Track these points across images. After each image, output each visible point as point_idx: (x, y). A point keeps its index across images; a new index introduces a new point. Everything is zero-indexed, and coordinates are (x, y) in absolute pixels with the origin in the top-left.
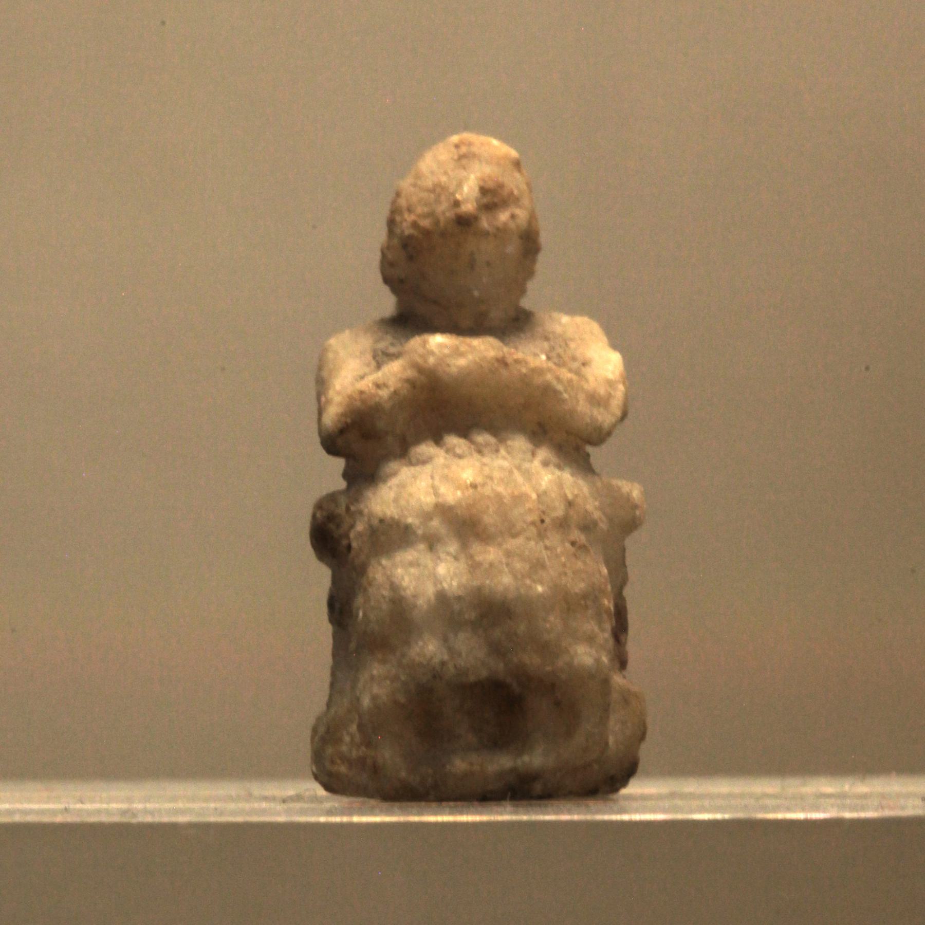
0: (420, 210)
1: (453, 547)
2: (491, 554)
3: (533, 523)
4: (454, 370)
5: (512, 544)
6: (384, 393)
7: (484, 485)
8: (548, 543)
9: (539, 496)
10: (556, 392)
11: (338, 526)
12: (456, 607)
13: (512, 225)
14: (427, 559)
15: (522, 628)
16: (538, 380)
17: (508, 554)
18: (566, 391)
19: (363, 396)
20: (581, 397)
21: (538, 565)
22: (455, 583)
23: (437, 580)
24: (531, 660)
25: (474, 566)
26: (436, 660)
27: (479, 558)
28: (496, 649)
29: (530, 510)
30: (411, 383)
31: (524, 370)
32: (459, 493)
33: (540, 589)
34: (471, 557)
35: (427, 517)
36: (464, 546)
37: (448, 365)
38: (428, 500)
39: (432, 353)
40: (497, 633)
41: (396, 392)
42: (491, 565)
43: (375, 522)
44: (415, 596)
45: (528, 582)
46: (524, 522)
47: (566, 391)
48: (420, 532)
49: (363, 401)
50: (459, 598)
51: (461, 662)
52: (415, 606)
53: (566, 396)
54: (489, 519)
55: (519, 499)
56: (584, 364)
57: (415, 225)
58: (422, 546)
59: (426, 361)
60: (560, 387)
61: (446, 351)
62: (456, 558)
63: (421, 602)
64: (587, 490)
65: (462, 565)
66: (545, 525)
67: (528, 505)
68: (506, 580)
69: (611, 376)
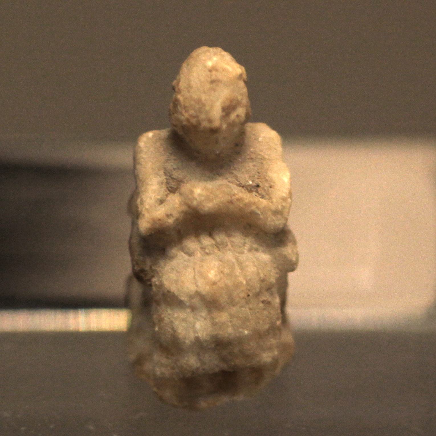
0: (192, 112)
1: (204, 313)
2: (223, 317)
3: (244, 298)
4: (206, 209)
5: (234, 310)
6: (171, 221)
7: (219, 281)
8: (251, 306)
9: (247, 282)
10: (257, 214)
11: (146, 275)
12: (205, 344)
13: (237, 121)
14: (191, 317)
15: (236, 350)
16: (249, 210)
17: (231, 316)
18: (262, 214)
19: (161, 222)
20: (270, 213)
21: (246, 320)
22: (204, 334)
23: (195, 332)
24: (239, 362)
25: (214, 324)
26: (195, 367)
27: (217, 320)
28: (223, 359)
29: (243, 291)
30: (185, 213)
31: (241, 205)
32: (208, 287)
33: (246, 332)
34: (212, 319)
35: (191, 297)
36: (210, 312)
37: (204, 206)
38: (192, 288)
39: (195, 199)
40: (224, 353)
41: (177, 219)
42: (223, 323)
43: (166, 291)
44: (185, 338)
45: (240, 330)
46: (240, 297)
47: (262, 214)
48: (188, 304)
49: (161, 225)
50: (206, 341)
51: (206, 367)
52: (184, 342)
53: (262, 217)
54: (223, 299)
55: (237, 286)
56: (271, 187)
57: (188, 120)
58: (188, 310)
59: (192, 203)
60: (259, 212)
61: (203, 198)
62: (205, 319)
63: (187, 341)
64: (273, 175)
65: (208, 322)
66: (249, 297)
67: (242, 288)
68: (230, 330)
69: (284, 195)
